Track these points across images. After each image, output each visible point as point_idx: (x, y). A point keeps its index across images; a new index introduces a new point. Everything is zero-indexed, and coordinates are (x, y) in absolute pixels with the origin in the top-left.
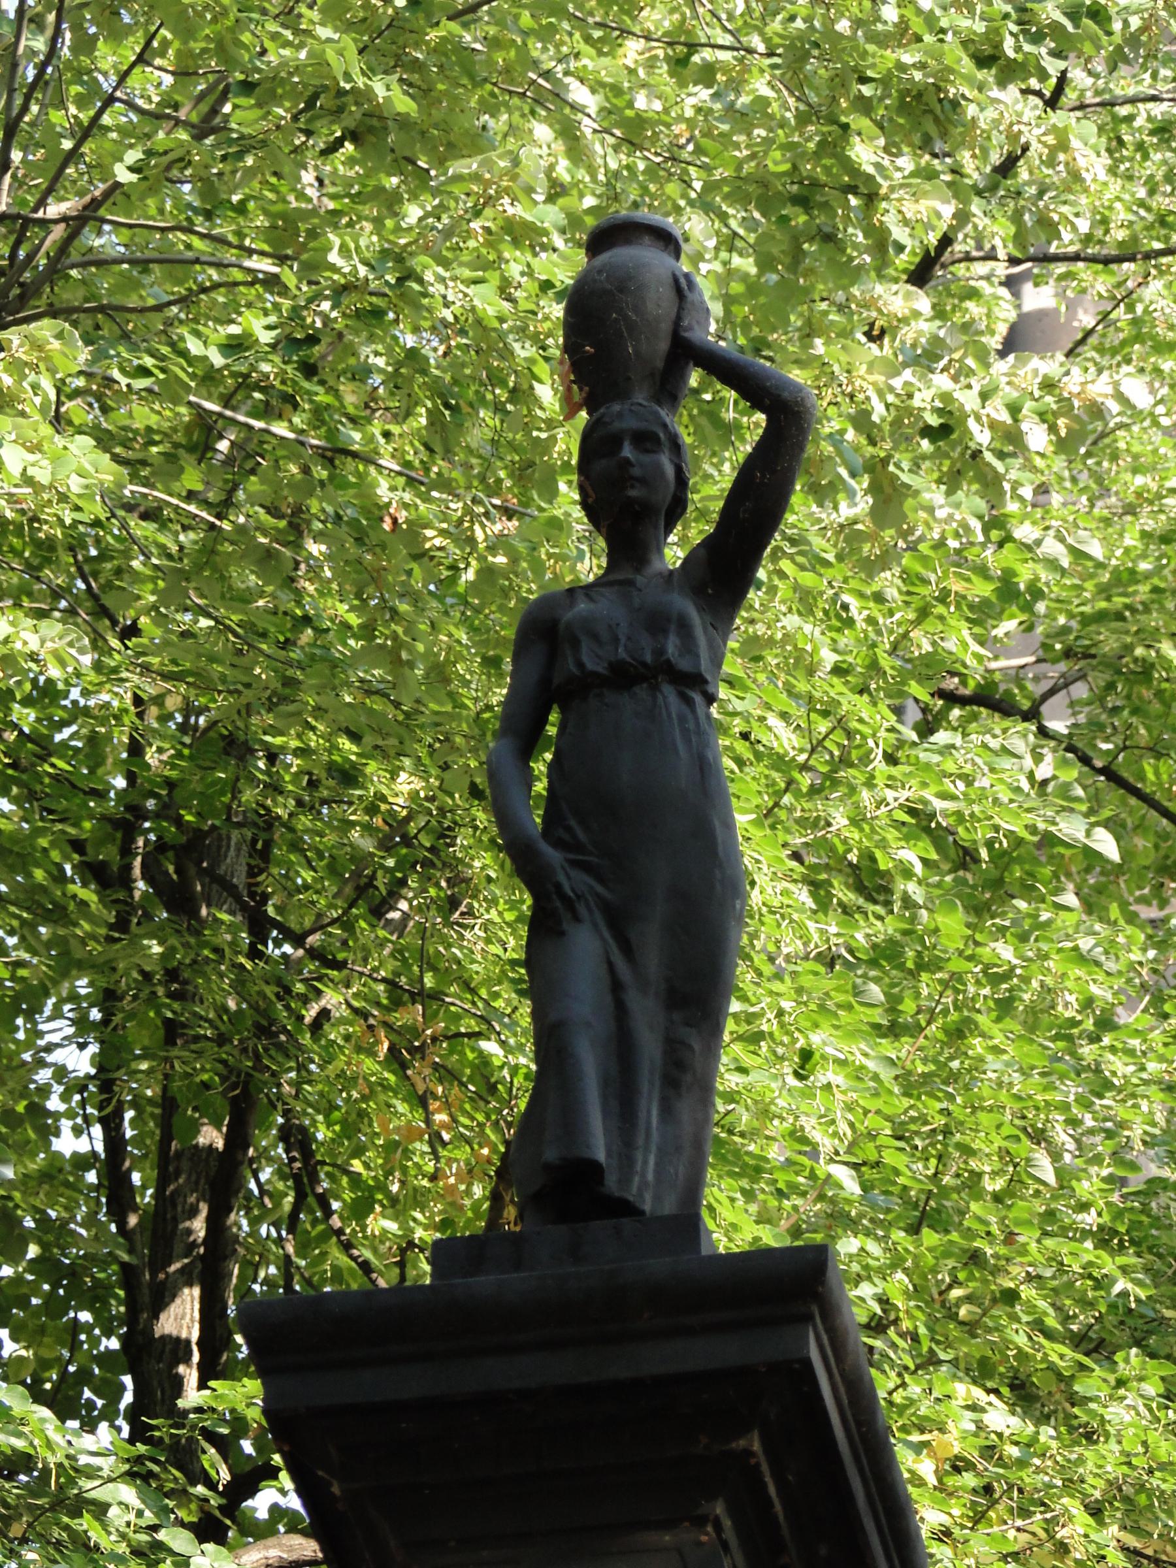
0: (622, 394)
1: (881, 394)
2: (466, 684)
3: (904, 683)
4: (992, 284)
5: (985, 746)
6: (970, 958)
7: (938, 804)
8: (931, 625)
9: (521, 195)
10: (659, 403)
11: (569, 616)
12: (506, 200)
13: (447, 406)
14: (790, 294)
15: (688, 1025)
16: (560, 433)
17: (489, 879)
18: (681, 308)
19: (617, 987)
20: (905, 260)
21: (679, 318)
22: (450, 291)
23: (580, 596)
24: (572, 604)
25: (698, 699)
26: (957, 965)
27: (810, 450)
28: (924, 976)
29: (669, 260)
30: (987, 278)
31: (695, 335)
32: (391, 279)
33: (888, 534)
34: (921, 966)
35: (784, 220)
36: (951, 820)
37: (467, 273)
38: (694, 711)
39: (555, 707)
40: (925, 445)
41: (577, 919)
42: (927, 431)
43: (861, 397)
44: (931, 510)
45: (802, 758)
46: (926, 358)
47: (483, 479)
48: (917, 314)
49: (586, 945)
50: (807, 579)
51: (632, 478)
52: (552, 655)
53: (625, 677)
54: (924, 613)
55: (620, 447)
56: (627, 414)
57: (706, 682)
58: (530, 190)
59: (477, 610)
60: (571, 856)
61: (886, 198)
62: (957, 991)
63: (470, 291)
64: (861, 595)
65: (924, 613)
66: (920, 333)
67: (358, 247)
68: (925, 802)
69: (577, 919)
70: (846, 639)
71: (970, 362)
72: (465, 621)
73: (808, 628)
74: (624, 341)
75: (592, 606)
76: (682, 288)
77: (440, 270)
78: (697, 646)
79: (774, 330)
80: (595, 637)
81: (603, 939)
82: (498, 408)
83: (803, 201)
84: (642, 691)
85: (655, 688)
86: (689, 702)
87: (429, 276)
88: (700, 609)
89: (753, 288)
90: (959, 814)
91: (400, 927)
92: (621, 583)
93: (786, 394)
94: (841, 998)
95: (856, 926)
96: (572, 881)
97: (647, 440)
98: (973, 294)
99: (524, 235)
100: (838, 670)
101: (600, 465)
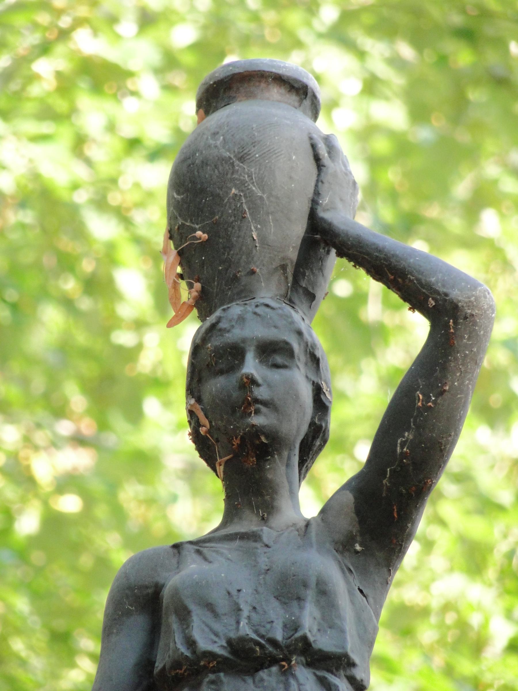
0: (245, 294)
2: (23, 663)
10: (291, 303)
14: (451, 155)
18: (319, 181)
23: (189, 553)
29: (303, 119)
35: (443, 60)
51: (256, 401)
52: (155, 631)
56: (248, 321)
57: (353, 665)
58: (113, 20)
59: (39, 570)
75: (206, 566)
76: (320, 156)
79: (428, 198)
80: (210, 607)
82: (67, 304)
83: (468, 35)
84: (269, 676)
85: (287, 673)
88: (346, 571)
89: (403, 147)
92: (243, 536)
99: (104, 77)
101: (216, 385)
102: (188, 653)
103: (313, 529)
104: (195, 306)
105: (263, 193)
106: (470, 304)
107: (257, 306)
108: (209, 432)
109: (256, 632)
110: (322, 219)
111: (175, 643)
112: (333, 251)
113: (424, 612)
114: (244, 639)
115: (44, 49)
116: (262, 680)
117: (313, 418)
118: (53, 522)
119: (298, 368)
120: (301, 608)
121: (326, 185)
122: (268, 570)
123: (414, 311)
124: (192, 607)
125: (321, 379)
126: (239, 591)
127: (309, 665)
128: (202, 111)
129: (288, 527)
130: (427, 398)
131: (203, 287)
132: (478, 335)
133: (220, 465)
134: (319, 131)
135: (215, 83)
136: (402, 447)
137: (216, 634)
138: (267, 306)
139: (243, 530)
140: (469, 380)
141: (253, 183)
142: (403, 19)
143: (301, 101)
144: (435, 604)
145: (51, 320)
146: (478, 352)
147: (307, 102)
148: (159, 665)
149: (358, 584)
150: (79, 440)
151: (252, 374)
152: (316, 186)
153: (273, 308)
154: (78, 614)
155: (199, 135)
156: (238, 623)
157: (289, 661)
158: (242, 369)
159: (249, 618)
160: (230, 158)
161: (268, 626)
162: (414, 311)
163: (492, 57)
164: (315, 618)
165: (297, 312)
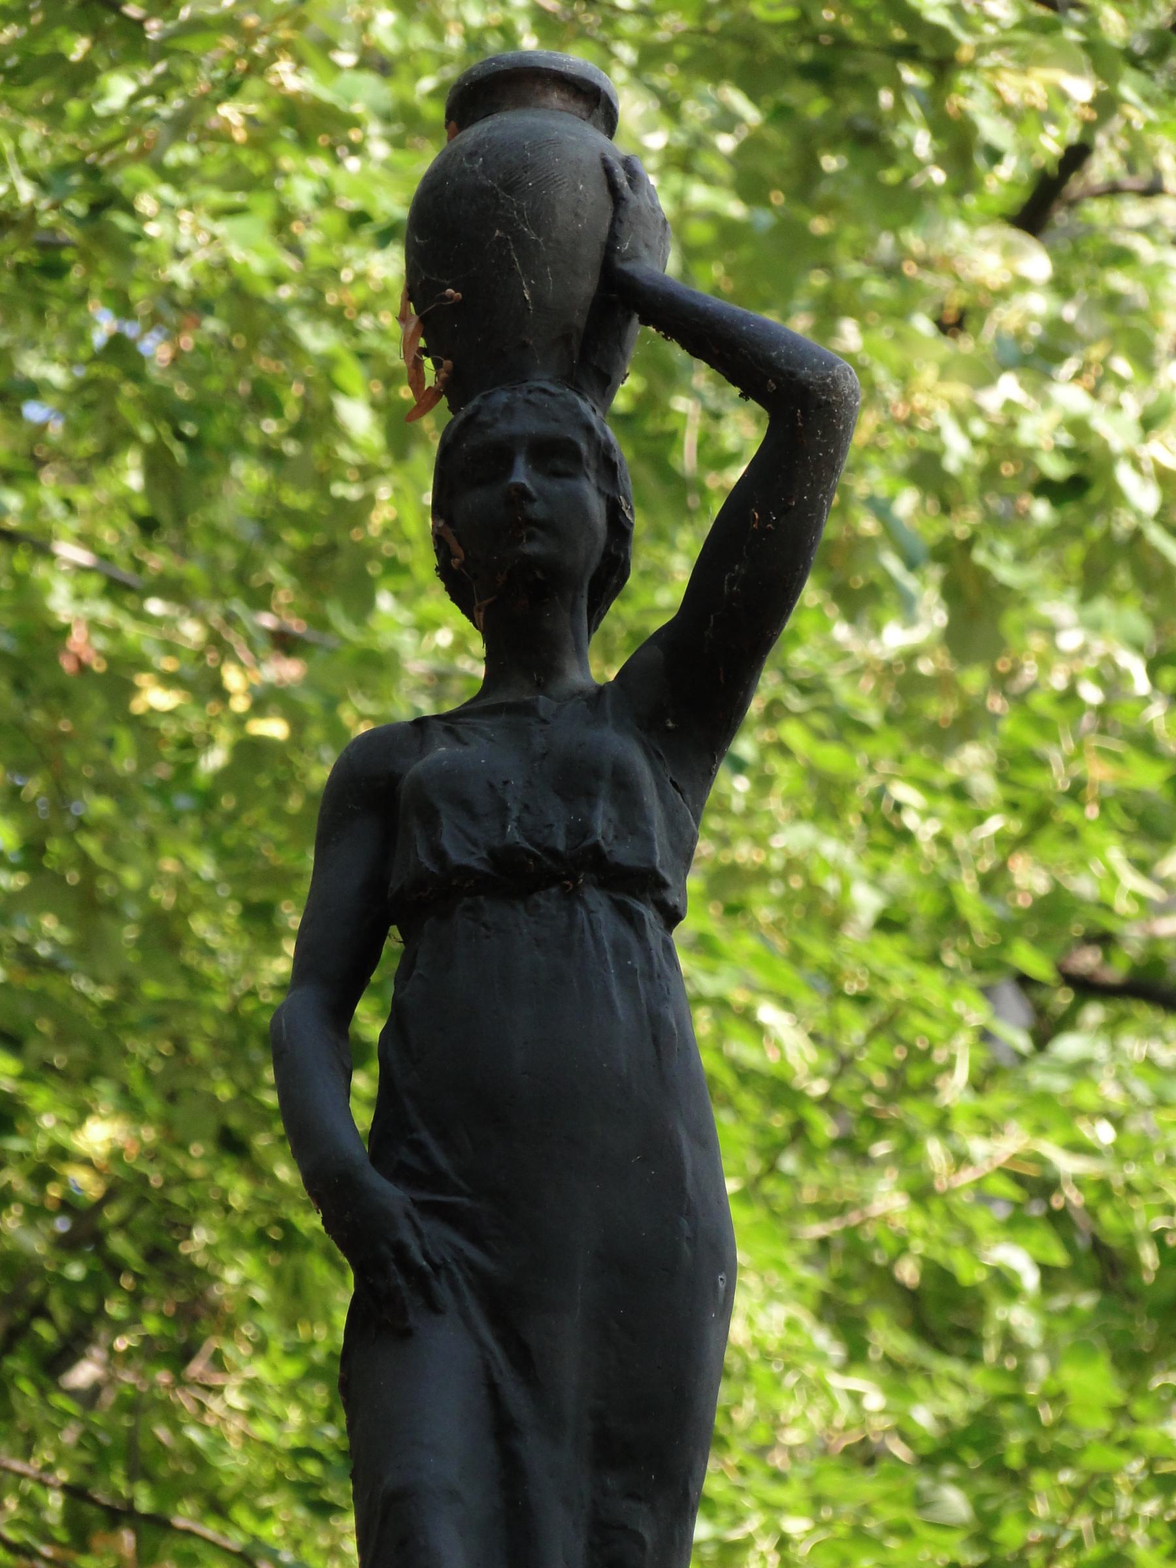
0: (515, 375)
1: (962, 419)
2: (210, 952)
3: (1004, 944)
4: (1154, 242)
5: (1149, 1062)
6: (1126, 1445)
7: (1067, 1165)
8: (1049, 843)
9: (311, 54)
10: (578, 389)
11: (418, 767)
12: (284, 66)
13: (180, 436)
15: (631, 1496)
16: (383, 492)
17: (253, 1304)
18: (616, 220)
19: (503, 1429)
20: (1005, 179)
22: (183, 233)
24: (423, 747)
25: (650, 915)
26: (1098, 1458)
27: (831, 529)
28: (1040, 1480)
30: (1145, 230)
31: (643, 267)
32: (78, 207)
33: (974, 679)
34: (1036, 1458)
36: (1092, 1195)
37: (216, 197)
38: (641, 937)
39: (394, 930)
40: (1042, 511)
41: (433, 1307)
42: (1045, 488)
43: (924, 424)
44: (1050, 630)
45: (818, 1088)
46: (1041, 356)
47: (241, 577)
48: (1023, 284)
49: (450, 1353)
50: (831, 757)
51: (530, 521)
53: (518, 875)
54: (1040, 819)
55: (509, 467)
56: (518, 412)
57: (664, 885)
58: (327, 45)
60: (425, 1196)
61: (971, 67)
62: (1097, 1509)
63: (222, 228)
64: (926, 787)
65: (1040, 819)
66: (1030, 317)
67: (18, 151)
68: (1040, 1160)
69: (433, 1307)
70: (898, 869)
71: (1122, 366)
72: (210, 839)
73: (831, 848)
74: (514, 280)
75: (459, 750)
76: (619, 184)
77: (167, 192)
78: (647, 820)
80: (465, 805)
81: (481, 1344)
82: (270, 455)
83: (821, 74)
84: (548, 901)
85: (572, 896)
86: (633, 920)
87: (146, 204)
88: (652, 755)
90: (1104, 1188)
91: (90, 1397)
94: (891, 1513)
95: (912, 1396)
96: (424, 1239)
97: (556, 455)
98: (1122, 257)
99: (314, 126)
100: (887, 924)
101: (475, 500)
102: (434, 869)
103: (608, 702)
104: (444, 393)
105: (539, 236)
106: (825, 388)
107: (530, 392)
108: (463, 565)
109: (528, 839)
110: (624, 274)
111: (417, 855)
112: (636, 316)
113: (762, 875)
114: (513, 850)
115: (232, 88)
116: (537, 906)
117: (607, 546)
118: (251, 752)
119: (588, 477)
120: (592, 807)
121: (626, 225)
122: (545, 754)
123: (747, 399)
124: (441, 805)
125: (619, 492)
126: (506, 783)
127: (602, 885)
128: (453, 124)
129: (573, 695)
130: (765, 518)
131: (455, 366)
132: (837, 432)
133: (479, 610)
134: (617, 152)
135: (471, 84)
136: (730, 586)
137: (475, 843)
138: (544, 391)
139: (511, 700)
140: (824, 493)
141: (524, 222)
142: (732, 52)
143: (590, 112)
144: (776, 863)
145: (248, 477)
146: (836, 452)
147: (599, 112)
148: (394, 885)
149: (670, 775)
150: (285, 643)
151: (523, 485)
152: (612, 226)
153: (552, 395)
154: (282, 878)
155: (449, 155)
156: (504, 827)
157: (575, 880)
158: (510, 476)
159: (519, 820)
160: (493, 188)
161: (546, 831)
162: (747, 399)
163: (854, 106)
164: (610, 821)
165: (585, 400)
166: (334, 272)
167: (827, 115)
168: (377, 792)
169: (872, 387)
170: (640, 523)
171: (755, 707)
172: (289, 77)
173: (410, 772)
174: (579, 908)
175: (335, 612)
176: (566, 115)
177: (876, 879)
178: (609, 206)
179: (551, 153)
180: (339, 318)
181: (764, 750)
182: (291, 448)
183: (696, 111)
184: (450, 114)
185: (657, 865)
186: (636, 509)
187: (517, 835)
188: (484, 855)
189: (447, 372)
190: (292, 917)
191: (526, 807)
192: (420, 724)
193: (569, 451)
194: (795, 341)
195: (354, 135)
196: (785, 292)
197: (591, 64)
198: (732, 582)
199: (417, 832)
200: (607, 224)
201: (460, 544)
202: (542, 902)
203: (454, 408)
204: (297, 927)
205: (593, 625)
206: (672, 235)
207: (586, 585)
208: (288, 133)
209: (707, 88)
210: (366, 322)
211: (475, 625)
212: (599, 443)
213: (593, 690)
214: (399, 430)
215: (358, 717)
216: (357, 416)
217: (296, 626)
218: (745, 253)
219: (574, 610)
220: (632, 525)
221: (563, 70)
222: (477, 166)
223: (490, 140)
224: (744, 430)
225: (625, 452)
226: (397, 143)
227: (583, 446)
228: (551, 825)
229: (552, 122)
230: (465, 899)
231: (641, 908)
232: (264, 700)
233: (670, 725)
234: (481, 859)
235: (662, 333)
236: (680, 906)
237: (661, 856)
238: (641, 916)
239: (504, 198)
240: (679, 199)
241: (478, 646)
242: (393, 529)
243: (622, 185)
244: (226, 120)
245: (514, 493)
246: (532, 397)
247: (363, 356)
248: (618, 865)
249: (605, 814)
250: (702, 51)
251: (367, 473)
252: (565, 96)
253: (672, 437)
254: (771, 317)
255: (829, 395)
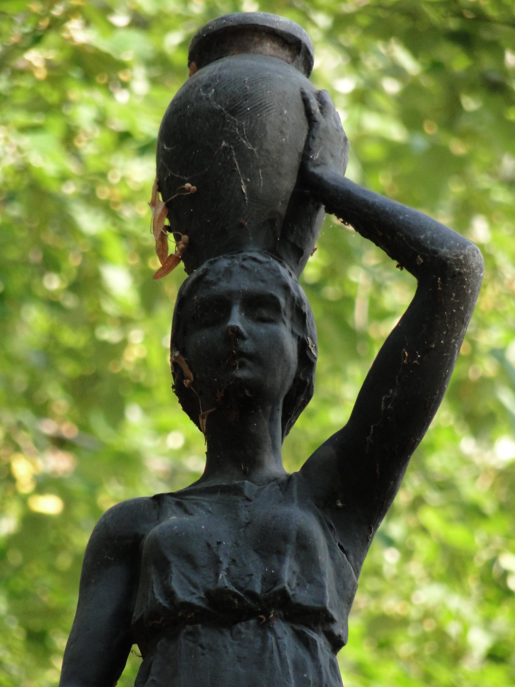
0: (233, 247)
11: (155, 530)
18: (310, 136)
21: (308, 149)
25: (321, 641)
31: (327, 172)
37: (21, 118)
38: (314, 658)
39: (135, 647)
50: (458, 535)
51: (241, 354)
53: (226, 610)
57: (331, 620)
73: (456, 602)
75: (186, 519)
76: (313, 112)
78: (321, 574)
80: (189, 559)
82: (53, 304)
84: (247, 629)
85: (265, 626)
86: (308, 645)
88: (326, 526)
93: (444, 251)
97: (261, 306)
99: (95, 68)
101: (202, 337)
102: (165, 604)
103: (295, 488)
106: (458, 263)
107: (244, 260)
108: (192, 384)
109: (235, 584)
110: (313, 175)
111: (154, 593)
112: (323, 208)
113: (403, 622)
114: (223, 592)
115: (36, 39)
116: (240, 632)
117: (297, 373)
118: (33, 522)
119: (284, 323)
120: (281, 562)
121: (317, 140)
122: (248, 523)
123: (402, 269)
124: (171, 558)
126: (219, 543)
128: (194, 64)
129: (269, 481)
130: (413, 356)
131: (190, 239)
132: (466, 294)
133: (203, 418)
135: (208, 35)
136: (386, 404)
137: (195, 586)
138: (255, 259)
139: (224, 484)
141: (243, 136)
143: (294, 57)
146: (465, 311)
147: (300, 58)
148: (136, 615)
149: (339, 540)
150: (60, 443)
152: (307, 140)
154: (54, 614)
155: (190, 87)
156: (217, 575)
157: (267, 615)
160: (222, 111)
161: (247, 579)
162: (402, 269)
163: (487, 62)
165: (284, 266)
166: (103, 175)
167: (469, 69)
168: (124, 547)
169: (495, 269)
170: (322, 363)
171: (402, 498)
172: (78, 32)
173: (150, 534)
174: (270, 635)
175: (99, 423)
176: (275, 59)
177: (487, 623)
178: (306, 127)
179: (264, 86)
180: (109, 209)
181: (410, 531)
182: (70, 302)
183: (371, 63)
184: (192, 57)
185: (327, 605)
186: (319, 349)
187: (226, 581)
188: (202, 595)
189: (184, 244)
190: (61, 642)
191: (234, 561)
192: (158, 498)
193: (272, 304)
194: (439, 228)
195: (122, 76)
196: (434, 194)
197: (295, 23)
198: (387, 402)
199: (154, 577)
200: (304, 139)
201: (191, 369)
202: (243, 630)
203: (189, 270)
204: (64, 649)
205: (285, 431)
206: (350, 149)
207: (281, 401)
208: (76, 74)
209: (380, 46)
210: (127, 213)
211: (200, 429)
212: (293, 298)
213: (284, 478)
214: (149, 291)
215: (112, 496)
216: (119, 281)
217: (69, 430)
218: (407, 167)
219: (272, 420)
220: (315, 358)
221: (274, 26)
222: (210, 95)
223: (220, 77)
224: (400, 294)
225: (314, 311)
226: (154, 81)
227: (282, 301)
228: (252, 575)
229: (267, 65)
230: (188, 626)
231: (314, 636)
232: (44, 484)
233: (340, 504)
234: (200, 598)
235: (341, 220)
236: (343, 636)
237: (331, 600)
238: (314, 642)
239: (229, 118)
240: (359, 127)
241: (201, 446)
242: (143, 363)
243: (315, 112)
244: (30, 63)
245: (230, 333)
246: (245, 264)
247: (124, 236)
248: (299, 605)
249: (290, 567)
250: (378, 20)
251: (125, 322)
252: (276, 46)
253: (348, 301)
254: (423, 212)
255: (461, 268)
